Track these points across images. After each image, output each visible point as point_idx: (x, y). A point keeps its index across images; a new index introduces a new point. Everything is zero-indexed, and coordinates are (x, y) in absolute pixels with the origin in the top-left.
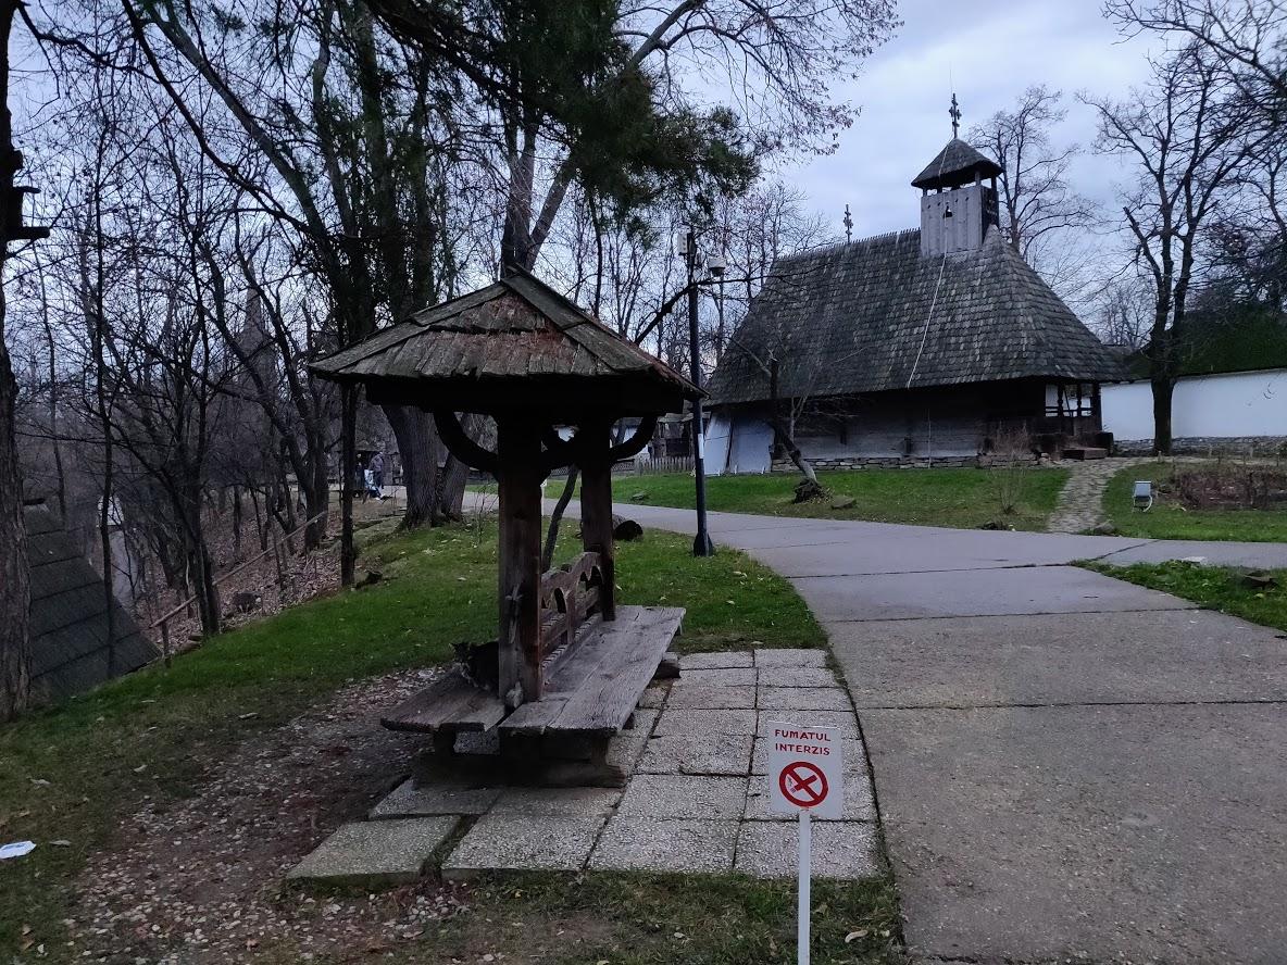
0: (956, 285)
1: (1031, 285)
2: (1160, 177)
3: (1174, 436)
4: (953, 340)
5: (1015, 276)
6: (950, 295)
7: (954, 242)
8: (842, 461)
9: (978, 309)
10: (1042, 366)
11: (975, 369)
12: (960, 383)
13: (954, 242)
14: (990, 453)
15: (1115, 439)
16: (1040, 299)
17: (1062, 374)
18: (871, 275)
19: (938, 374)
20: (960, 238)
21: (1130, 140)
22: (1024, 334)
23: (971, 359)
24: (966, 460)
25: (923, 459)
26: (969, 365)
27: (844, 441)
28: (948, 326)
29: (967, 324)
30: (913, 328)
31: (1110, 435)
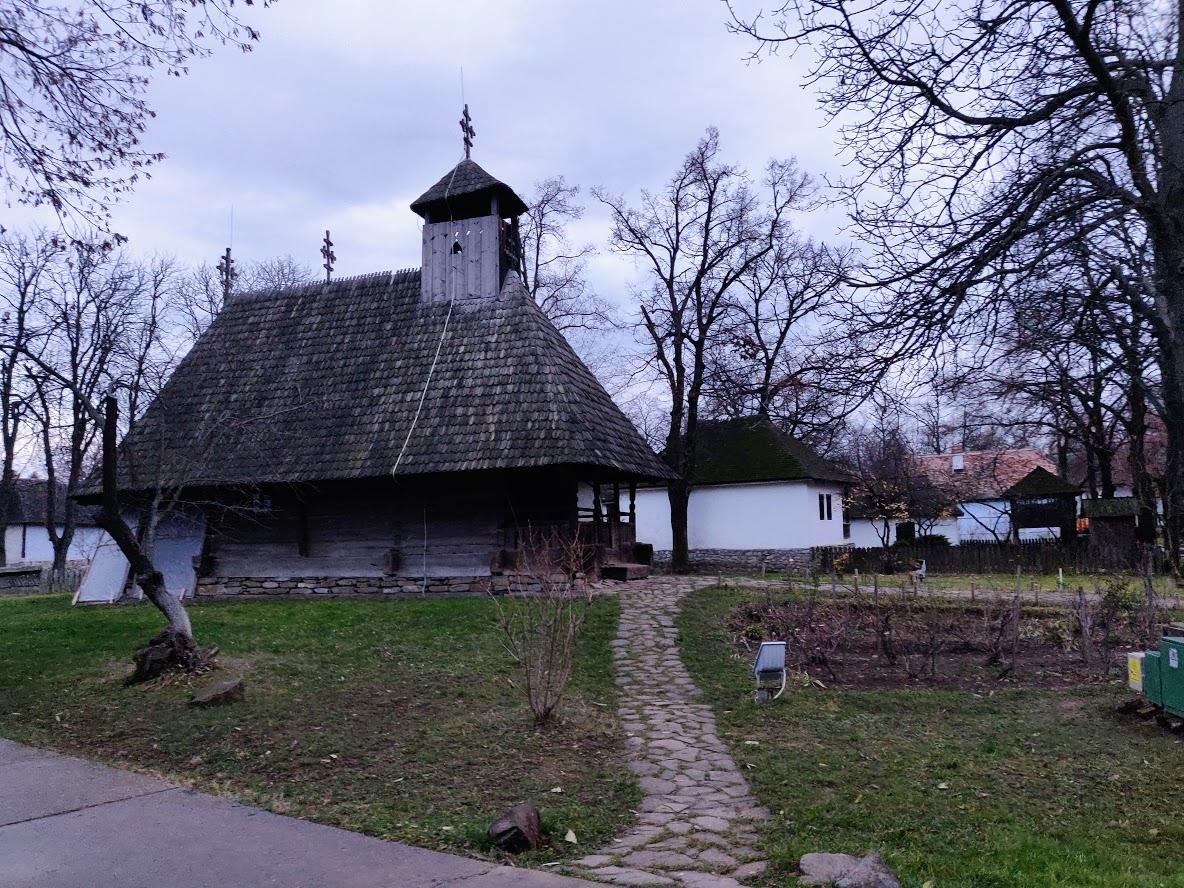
0: (465, 340)
1: (560, 350)
2: (670, 283)
3: (690, 547)
4: (460, 411)
5: (541, 335)
6: (457, 353)
7: (465, 285)
8: (302, 580)
9: (494, 371)
10: (576, 449)
11: (491, 452)
12: (467, 470)
13: (465, 285)
14: (507, 573)
15: (655, 549)
16: (571, 367)
17: (603, 461)
18: (354, 322)
19: (437, 457)
20: (471, 280)
21: (642, 244)
22: (554, 407)
23: (483, 437)
24: (474, 581)
25: (415, 580)
26: (481, 445)
27: (305, 552)
28: (453, 392)
29: (479, 391)
30: (406, 392)
31: (649, 547)
